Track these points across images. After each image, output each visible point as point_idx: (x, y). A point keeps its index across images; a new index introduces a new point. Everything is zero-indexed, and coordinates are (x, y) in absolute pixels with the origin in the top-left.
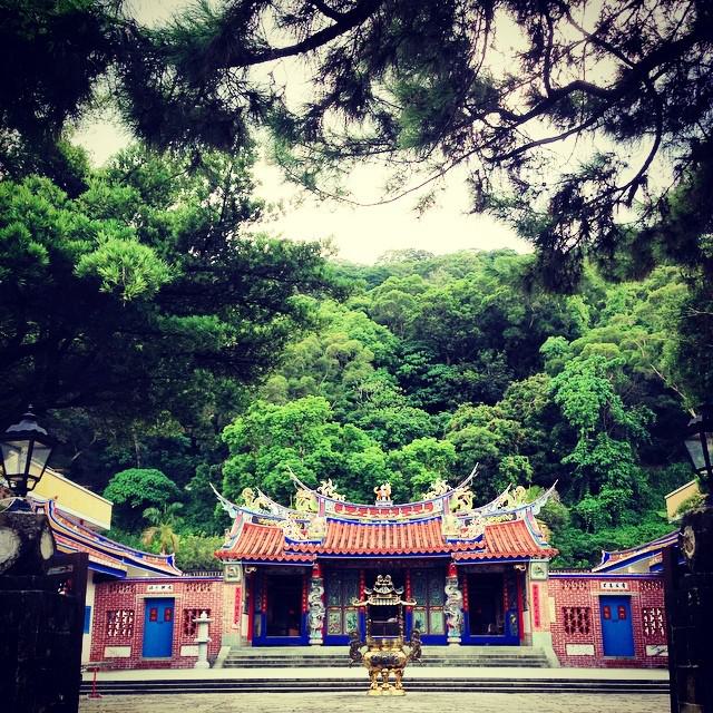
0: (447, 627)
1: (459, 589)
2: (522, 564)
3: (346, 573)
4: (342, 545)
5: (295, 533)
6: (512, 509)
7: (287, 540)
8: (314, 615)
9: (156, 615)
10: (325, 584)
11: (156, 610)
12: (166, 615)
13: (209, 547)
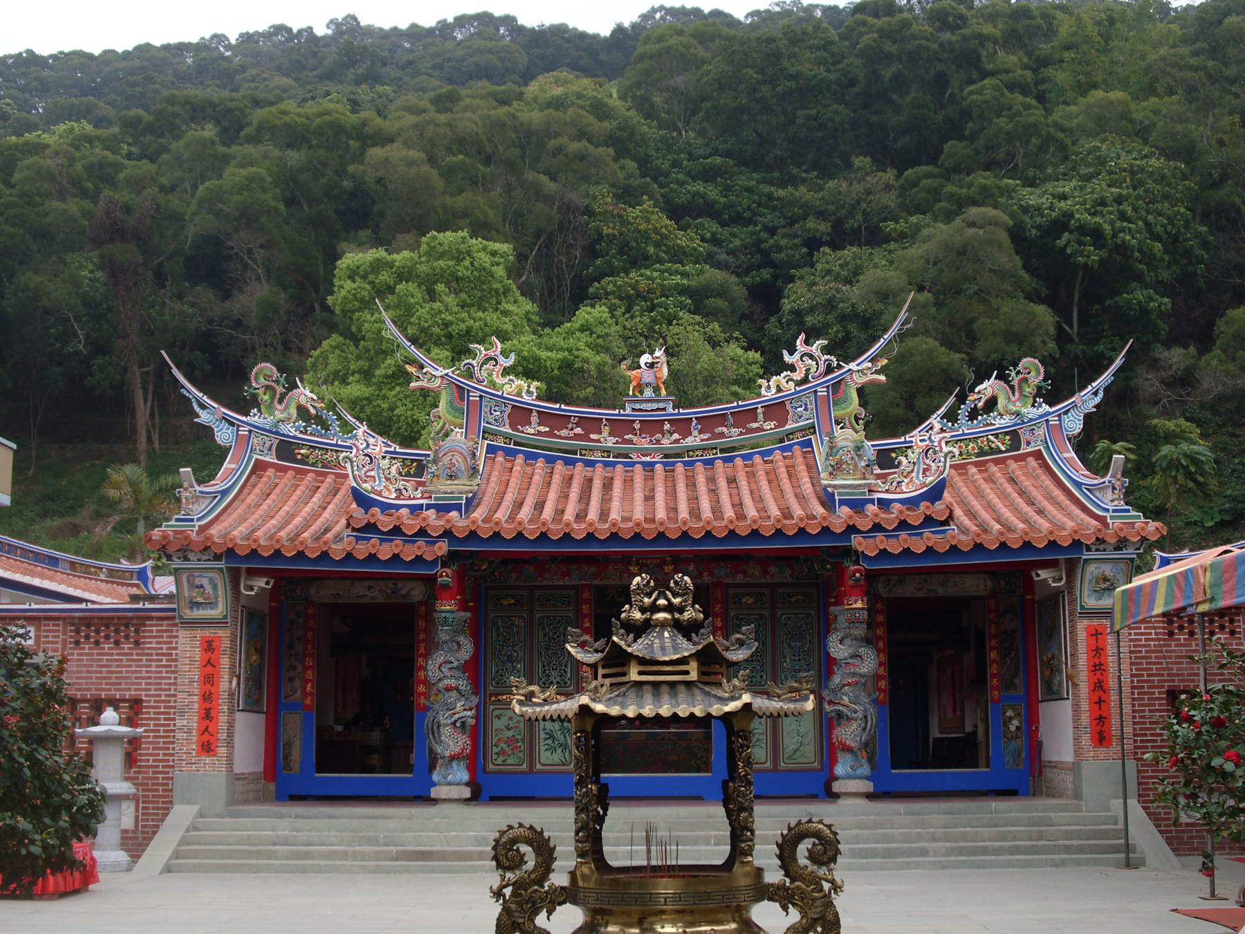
1: (868, 641)
2: (1052, 564)
3: (544, 593)
4: (525, 513)
6: (1002, 422)
7: (361, 499)
8: (444, 718)
10: (476, 630)
13: (84, 162)
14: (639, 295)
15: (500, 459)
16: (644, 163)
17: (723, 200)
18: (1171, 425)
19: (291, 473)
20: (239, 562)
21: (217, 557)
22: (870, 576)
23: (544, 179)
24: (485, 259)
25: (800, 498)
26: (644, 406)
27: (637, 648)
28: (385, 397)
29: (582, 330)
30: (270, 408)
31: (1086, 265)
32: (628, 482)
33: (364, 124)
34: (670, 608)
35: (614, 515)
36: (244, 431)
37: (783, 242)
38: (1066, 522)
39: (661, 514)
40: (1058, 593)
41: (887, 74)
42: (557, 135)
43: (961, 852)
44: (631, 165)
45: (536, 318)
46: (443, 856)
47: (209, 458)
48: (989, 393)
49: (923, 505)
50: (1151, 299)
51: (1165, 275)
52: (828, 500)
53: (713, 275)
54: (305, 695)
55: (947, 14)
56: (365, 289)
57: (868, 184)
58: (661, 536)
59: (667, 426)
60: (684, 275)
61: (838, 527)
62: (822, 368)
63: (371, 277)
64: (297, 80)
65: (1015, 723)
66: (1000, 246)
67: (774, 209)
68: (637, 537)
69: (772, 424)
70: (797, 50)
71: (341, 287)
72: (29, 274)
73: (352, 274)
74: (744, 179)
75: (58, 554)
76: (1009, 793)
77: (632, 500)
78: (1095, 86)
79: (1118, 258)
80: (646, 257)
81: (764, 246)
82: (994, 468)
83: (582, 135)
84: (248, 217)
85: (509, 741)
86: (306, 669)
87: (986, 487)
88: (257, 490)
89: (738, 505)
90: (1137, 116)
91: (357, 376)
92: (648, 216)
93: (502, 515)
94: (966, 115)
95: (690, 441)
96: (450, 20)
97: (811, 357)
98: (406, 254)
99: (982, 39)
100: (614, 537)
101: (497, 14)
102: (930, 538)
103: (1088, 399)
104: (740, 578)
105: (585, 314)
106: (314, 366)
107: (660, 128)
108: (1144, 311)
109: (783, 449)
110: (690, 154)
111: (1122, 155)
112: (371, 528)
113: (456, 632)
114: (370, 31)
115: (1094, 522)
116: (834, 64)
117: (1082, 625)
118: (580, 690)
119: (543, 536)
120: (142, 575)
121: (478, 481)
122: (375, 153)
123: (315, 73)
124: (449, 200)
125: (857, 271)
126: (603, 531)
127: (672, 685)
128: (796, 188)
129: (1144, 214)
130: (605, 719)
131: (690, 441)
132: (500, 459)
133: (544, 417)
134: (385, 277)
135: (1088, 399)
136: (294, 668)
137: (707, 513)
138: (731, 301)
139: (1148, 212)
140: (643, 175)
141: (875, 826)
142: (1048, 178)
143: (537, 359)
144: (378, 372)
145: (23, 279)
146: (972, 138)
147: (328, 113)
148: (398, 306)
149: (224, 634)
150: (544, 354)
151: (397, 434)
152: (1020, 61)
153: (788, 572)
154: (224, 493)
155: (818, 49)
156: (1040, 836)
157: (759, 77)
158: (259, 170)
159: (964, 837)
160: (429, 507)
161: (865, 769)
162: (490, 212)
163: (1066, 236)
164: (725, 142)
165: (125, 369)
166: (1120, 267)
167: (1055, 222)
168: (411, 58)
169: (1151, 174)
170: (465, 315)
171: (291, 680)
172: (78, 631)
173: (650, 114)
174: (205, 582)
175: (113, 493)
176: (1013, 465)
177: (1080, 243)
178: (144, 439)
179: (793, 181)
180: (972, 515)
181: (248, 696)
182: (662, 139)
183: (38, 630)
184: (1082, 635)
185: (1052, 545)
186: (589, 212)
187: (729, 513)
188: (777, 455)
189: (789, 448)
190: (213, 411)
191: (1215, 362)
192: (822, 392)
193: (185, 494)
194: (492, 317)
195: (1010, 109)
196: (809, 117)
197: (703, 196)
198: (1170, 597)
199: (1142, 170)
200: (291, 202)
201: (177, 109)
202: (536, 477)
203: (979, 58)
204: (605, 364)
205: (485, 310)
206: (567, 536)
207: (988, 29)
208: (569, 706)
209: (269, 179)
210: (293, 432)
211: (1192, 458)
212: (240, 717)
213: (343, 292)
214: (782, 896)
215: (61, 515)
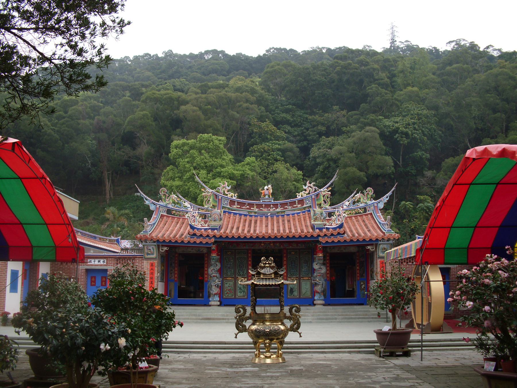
0: (313, 293)
1: (324, 264)
2: (372, 245)
4: (234, 231)
5: (199, 224)
6: (362, 205)
7: (192, 227)
9: (95, 282)
10: (221, 261)
11: (95, 277)
12: (102, 282)
14: (265, 151)
15: (227, 215)
16: (266, 107)
17: (292, 119)
18: (422, 197)
19: (170, 218)
20: (159, 243)
21: (154, 242)
22: (323, 247)
23: (235, 113)
24: (217, 142)
25: (306, 226)
26: (266, 200)
27: (262, 271)
28: (186, 185)
29: (247, 165)
30: (165, 200)
31: (403, 144)
32: (261, 221)
33: (179, 97)
34: (269, 264)
35: (257, 232)
36: (158, 206)
37: (311, 133)
38: (375, 234)
39: (270, 231)
40: (373, 252)
41: (345, 78)
42: (239, 102)
43: (346, 318)
44: (263, 108)
45: (233, 160)
46: (213, 319)
47: (149, 214)
48: (358, 197)
49: (338, 229)
50: (423, 154)
51: (428, 147)
52: (313, 227)
53: (288, 145)
54: (175, 277)
55: (363, 61)
56: (180, 151)
57: (337, 115)
58: (270, 237)
59: (272, 206)
60: (279, 144)
61: (315, 235)
62: (314, 190)
63: (182, 148)
64: (153, 73)
65: (363, 286)
66: (376, 139)
67: (308, 122)
68: (263, 237)
69: (300, 205)
70: (315, 71)
71: (173, 151)
72: (74, 143)
73: (176, 147)
74: (299, 113)
75: (96, 235)
76: (362, 304)
77: (263, 227)
78: (408, 85)
79: (413, 142)
80: (267, 139)
81: (305, 134)
82: (359, 218)
83: (247, 101)
84: (142, 127)
85: (229, 290)
86: (175, 271)
87: (356, 223)
88: (162, 223)
89: (290, 229)
90: (421, 95)
91: (178, 179)
92: (268, 126)
93: (228, 231)
94: (366, 96)
95: (278, 210)
96: (203, 52)
97: (311, 187)
98: (193, 140)
99: (374, 69)
100: (257, 237)
101: (218, 50)
102: (339, 238)
103: (385, 199)
104: (291, 247)
105: (248, 159)
106: (164, 175)
107: (272, 95)
108: (421, 158)
109: (303, 212)
110: (282, 104)
111: (415, 108)
112: (195, 235)
113: (216, 262)
114: (176, 55)
115: (382, 234)
116: (327, 76)
117: (379, 260)
118: (252, 279)
119: (239, 237)
120: (117, 241)
121: (222, 222)
122: (183, 108)
123: (159, 71)
124: (205, 122)
125: (333, 145)
126: (255, 236)
127: (269, 278)
128: (315, 116)
129: (421, 128)
130: (256, 285)
131: (278, 210)
132: (227, 215)
133: (239, 203)
134: (186, 148)
135: (385, 199)
136: (172, 270)
137: (282, 231)
138: (294, 153)
139: (423, 127)
140: (266, 112)
141: (324, 312)
142: (393, 116)
143: (233, 174)
144: (184, 178)
145: (72, 145)
146: (370, 102)
147: (168, 94)
148: (190, 157)
149: (156, 262)
150: (235, 172)
151: (190, 196)
152: (386, 75)
153: (304, 246)
154: (154, 224)
155: (322, 71)
156: (366, 315)
157: (303, 80)
158: (147, 112)
159: (346, 315)
160: (209, 229)
161: (323, 298)
162: (218, 125)
163: (397, 135)
164: (293, 100)
165: (102, 172)
166: (413, 145)
167: (394, 130)
168: (190, 65)
169: (424, 115)
170: (211, 160)
171: (171, 274)
172: (117, 261)
173: (269, 90)
174: (151, 248)
175: (107, 216)
176: (364, 217)
177: (402, 137)
178: (108, 195)
179: (312, 113)
180: (351, 231)
181: (161, 278)
182: (273, 99)
183: (107, 260)
184: (379, 263)
185: (371, 240)
186: (249, 124)
187: (287, 231)
188: (301, 214)
189: (304, 212)
190: (149, 201)
191: (441, 176)
192: (313, 197)
193: (145, 225)
194: (219, 161)
195: (381, 94)
196: (319, 93)
197: (285, 118)
198: (394, 256)
199: (421, 114)
200: (155, 120)
201: (118, 88)
202: (237, 220)
203: (373, 75)
204: (254, 175)
205: (217, 158)
206: (245, 237)
207: (376, 66)
208: (250, 282)
209: (150, 115)
210: (171, 207)
211: (428, 207)
212: (159, 283)
213: (173, 153)
214: (290, 318)
215: (83, 219)
